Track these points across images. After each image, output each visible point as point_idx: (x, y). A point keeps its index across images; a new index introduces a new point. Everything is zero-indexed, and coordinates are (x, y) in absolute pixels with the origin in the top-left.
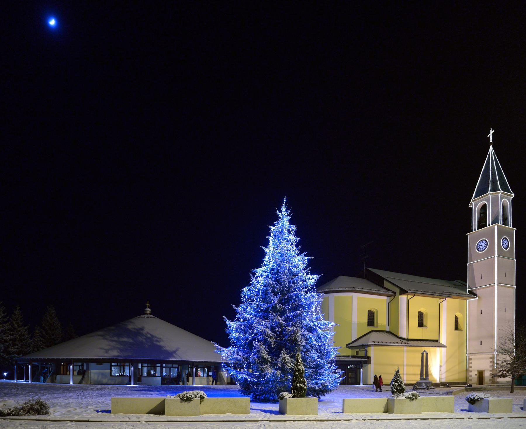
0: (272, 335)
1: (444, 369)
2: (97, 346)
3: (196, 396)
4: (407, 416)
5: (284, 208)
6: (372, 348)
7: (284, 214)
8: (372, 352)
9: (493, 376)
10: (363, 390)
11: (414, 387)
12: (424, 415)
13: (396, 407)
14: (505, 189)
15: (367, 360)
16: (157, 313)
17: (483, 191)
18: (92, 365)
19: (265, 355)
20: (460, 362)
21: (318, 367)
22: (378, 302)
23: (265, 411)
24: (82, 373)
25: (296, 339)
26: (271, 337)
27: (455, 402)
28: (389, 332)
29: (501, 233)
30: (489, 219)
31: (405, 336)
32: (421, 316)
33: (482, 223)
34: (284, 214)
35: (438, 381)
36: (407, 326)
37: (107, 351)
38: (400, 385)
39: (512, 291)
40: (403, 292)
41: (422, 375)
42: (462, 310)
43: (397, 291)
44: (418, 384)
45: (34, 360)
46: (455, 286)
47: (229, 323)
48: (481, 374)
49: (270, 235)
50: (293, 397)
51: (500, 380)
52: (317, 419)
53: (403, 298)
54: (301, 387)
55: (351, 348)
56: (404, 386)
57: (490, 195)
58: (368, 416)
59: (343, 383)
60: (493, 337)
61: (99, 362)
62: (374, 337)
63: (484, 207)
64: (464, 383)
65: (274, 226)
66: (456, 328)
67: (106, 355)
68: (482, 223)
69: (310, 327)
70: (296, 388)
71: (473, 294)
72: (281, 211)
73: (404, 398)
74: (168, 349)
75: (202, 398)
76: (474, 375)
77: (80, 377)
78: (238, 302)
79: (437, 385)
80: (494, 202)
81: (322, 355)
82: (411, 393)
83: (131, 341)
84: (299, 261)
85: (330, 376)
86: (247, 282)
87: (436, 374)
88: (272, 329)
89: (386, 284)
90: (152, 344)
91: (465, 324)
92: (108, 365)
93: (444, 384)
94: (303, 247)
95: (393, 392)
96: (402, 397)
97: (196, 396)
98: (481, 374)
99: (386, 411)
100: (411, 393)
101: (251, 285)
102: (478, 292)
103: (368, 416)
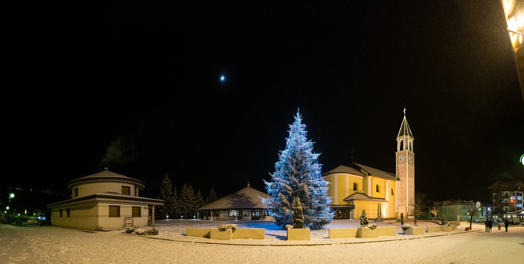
0: (290, 188)
1: (387, 212)
2: (223, 203)
3: (228, 228)
4: (370, 240)
5: (298, 114)
6: (356, 201)
7: (298, 119)
8: (356, 203)
9: (408, 215)
10: (33, 225)
11: (375, 220)
12: (380, 238)
13: (363, 234)
14: (410, 135)
15: (353, 207)
16: (252, 186)
17: (402, 134)
18: (221, 211)
19: (285, 201)
20: (394, 209)
21: (319, 209)
22: (358, 179)
23: (278, 237)
24: (217, 215)
25: (304, 191)
26: (289, 190)
27: (397, 228)
28: (363, 194)
29: (409, 154)
30: (404, 147)
31: (370, 196)
32: (377, 186)
33: (402, 149)
34: (298, 119)
35: (385, 218)
36: (371, 192)
37: (226, 205)
38: (365, 220)
39: (413, 180)
40: (370, 174)
41: (378, 214)
42: (394, 186)
43: (367, 174)
44: (377, 219)
45: (199, 211)
46: (391, 175)
47: (266, 183)
48: (402, 214)
49: (290, 130)
50: (294, 228)
51: (409, 217)
52: (308, 244)
53: (370, 178)
54: (299, 221)
55: (346, 201)
56: (368, 220)
57: (404, 136)
58: (344, 240)
59: (334, 218)
60: (406, 199)
61: (224, 210)
62: (356, 196)
63: (402, 142)
64: (396, 219)
65: (292, 125)
66: (392, 194)
67: (429, 226)
68: (402, 149)
69: (315, 185)
70: (295, 222)
71: (398, 179)
72: (296, 116)
73: (367, 228)
74: (254, 202)
75: (234, 229)
76: (399, 216)
77: (216, 217)
78: (273, 170)
79: (385, 219)
80: (406, 140)
81: (322, 201)
82: (372, 225)
83: (238, 199)
84: (308, 144)
85: (327, 214)
86: (278, 159)
87: (384, 215)
88: (291, 185)
89: (362, 171)
90: (248, 201)
91: (396, 192)
92: (227, 211)
93: (388, 219)
94: (309, 137)
95: (361, 224)
96: (366, 227)
97: (228, 228)
98: (402, 214)
99: (358, 236)
100: (372, 225)
101: (280, 161)
102: (400, 178)
103: (344, 240)
